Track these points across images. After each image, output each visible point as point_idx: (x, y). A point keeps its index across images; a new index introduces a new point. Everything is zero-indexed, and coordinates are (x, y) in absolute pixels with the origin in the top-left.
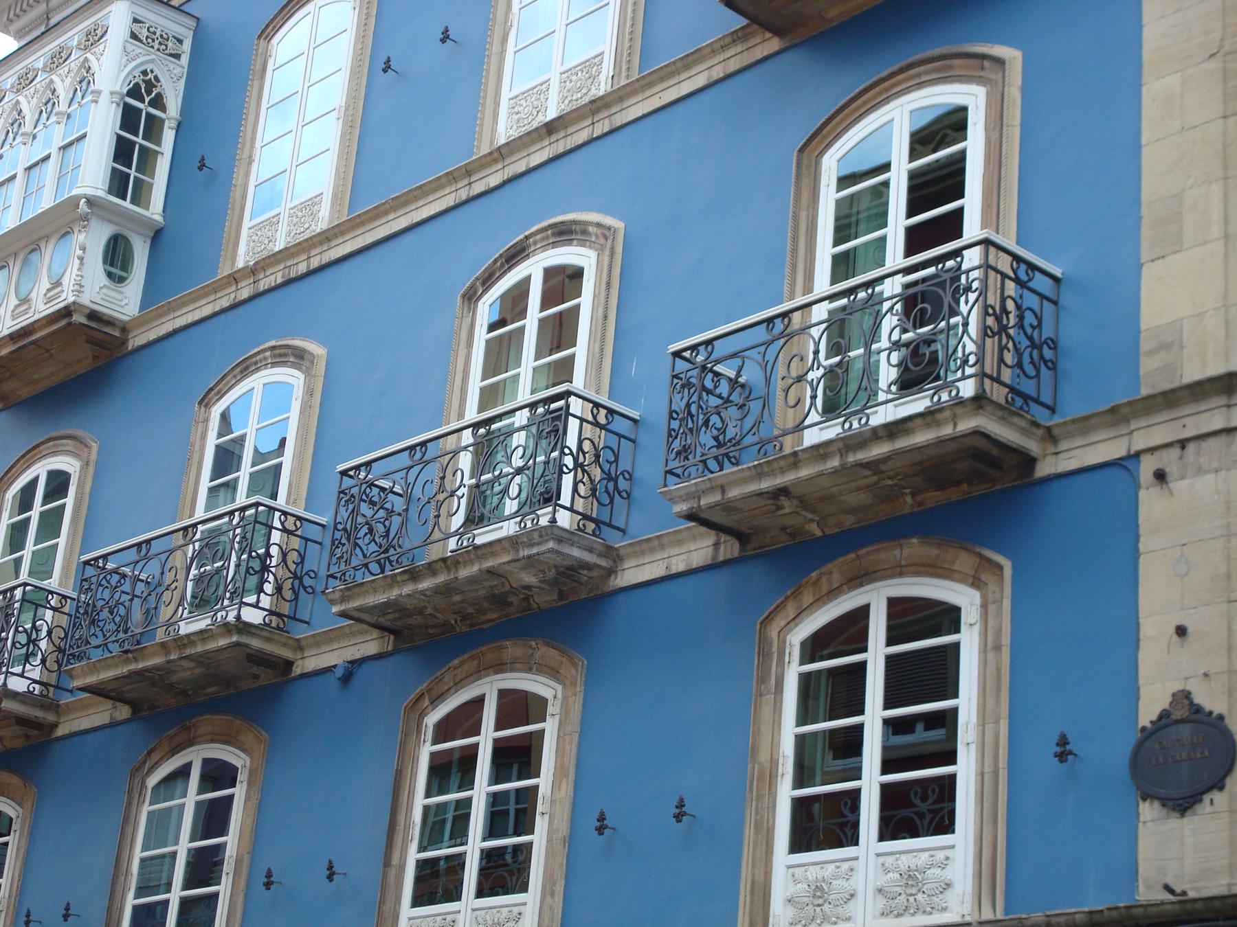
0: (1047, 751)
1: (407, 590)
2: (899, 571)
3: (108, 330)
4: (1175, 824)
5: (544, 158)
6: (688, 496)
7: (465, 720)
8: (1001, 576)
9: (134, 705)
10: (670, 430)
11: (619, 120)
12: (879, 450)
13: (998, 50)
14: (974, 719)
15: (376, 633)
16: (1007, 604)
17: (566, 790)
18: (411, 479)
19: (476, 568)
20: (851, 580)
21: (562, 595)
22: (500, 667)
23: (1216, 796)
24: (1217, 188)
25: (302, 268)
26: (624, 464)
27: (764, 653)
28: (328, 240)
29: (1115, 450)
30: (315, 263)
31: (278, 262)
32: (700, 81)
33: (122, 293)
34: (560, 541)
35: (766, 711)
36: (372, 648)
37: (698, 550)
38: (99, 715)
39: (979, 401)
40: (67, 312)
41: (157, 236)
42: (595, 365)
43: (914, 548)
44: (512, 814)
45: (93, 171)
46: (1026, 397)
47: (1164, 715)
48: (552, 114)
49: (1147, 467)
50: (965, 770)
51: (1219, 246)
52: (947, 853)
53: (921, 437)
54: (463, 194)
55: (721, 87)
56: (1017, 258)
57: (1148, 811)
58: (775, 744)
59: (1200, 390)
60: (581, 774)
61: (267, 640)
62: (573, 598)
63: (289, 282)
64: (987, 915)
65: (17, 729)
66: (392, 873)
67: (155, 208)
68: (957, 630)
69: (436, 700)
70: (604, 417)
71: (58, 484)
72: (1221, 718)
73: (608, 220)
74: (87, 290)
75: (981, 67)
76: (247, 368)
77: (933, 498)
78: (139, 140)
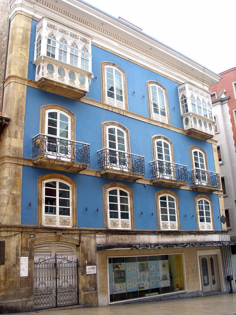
2: (171, 194)
36: (149, 184)
60: (179, 208)
76: (113, 124)
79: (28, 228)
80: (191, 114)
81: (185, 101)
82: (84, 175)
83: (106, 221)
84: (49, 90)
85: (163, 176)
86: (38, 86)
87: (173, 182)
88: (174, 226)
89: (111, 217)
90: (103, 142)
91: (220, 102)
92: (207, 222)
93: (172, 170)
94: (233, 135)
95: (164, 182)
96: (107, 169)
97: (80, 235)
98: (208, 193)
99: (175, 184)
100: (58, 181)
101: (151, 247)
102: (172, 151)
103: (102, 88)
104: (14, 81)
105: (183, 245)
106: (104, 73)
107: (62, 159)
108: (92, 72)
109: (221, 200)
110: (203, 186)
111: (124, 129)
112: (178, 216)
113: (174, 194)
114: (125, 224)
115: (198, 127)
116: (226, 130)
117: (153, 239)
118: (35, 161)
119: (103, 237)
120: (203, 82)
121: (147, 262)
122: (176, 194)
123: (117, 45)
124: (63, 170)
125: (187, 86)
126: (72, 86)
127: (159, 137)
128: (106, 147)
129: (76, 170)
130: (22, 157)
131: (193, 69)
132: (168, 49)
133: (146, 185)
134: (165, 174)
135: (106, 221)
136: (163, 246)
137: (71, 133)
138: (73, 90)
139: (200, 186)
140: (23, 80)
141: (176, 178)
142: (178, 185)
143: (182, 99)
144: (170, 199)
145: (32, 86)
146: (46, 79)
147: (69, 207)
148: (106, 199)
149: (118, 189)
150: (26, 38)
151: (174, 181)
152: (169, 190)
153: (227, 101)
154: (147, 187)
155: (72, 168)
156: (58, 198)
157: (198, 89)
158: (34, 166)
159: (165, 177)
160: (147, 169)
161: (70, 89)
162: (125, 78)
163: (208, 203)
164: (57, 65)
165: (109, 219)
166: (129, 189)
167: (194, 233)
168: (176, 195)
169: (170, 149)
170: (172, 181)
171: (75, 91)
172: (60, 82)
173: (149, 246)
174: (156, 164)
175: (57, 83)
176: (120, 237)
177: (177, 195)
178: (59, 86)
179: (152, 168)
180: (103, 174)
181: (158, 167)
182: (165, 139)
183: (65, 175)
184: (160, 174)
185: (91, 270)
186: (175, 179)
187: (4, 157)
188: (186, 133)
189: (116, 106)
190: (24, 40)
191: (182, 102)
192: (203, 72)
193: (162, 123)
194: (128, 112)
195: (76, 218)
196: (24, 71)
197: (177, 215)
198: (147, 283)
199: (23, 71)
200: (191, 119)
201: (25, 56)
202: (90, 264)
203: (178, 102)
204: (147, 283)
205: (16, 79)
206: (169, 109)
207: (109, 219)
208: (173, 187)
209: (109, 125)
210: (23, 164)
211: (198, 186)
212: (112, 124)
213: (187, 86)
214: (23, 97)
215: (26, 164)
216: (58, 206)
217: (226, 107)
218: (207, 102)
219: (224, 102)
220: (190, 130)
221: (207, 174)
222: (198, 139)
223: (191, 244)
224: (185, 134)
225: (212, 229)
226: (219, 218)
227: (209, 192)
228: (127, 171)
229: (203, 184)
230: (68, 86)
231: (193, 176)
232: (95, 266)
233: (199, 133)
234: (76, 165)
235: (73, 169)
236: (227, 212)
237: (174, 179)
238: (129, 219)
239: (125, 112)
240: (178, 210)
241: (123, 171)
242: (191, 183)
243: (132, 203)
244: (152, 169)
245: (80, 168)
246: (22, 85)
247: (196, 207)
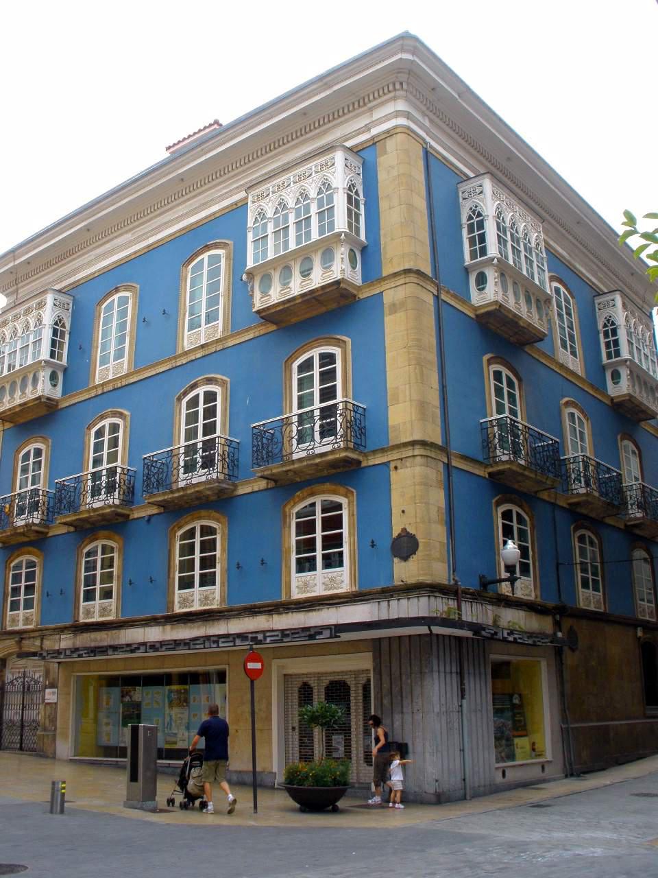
0: (368, 546)
1: (170, 496)
2: (323, 492)
3: (52, 403)
4: (403, 564)
5: (201, 356)
6: (261, 471)
7: (191, 534)
8: (353, 495)
9: (75, 527)
10: (253, 451)
12: (318, 460)
13: (344, 338)
14: (347, 535)
15: (156, 507)
16: (355, 503)
17: (225, 556)
18: (168, 461)
21: (219, 497)
22: (200, 518)
23: (413, 556)
24: (407, 386)
25: (119, 385)
26: (236, 457)
27: (285, 516)
28: (128, 376)
29: (384, 460)
30: (124, 384)
31: (111, 383)
32: (251, 336)
33: (310, 279)
34: (219, 483)
35: (287, 532)
37: (262, 484)
38: (64, 530)
39: (346, 449)
40: (39, 398)
41: (65, 370)
42: (223, 424)
43: (327, 486)
44: (208, 562)
45: (45, 354)
46: (358, 445)
47: (399, 535)
48: (203, 342)
49: (392, 465)
50: (346, 549)
51: (409, 403)
53: (330, 457)
56: (354, 405)
57: (396, 560)
58: (290, 543)
59: (405, 445)
60: (230, 551)
61: (122, 509)
62: (222, 497)
63: (114, 390)
64: (354, 589)
65: (35, 534)
66: (171, 580)
67: (64, 362)
68: (341, 510)
69: (180, 528)
70: (229, 443)
71: (38, 453)
72: (414, 535)
73: (224, 378)
74: (46, 390)
75: (340, 343)
77: (333, 471)
78: (58, 339)
80: (628, 363)
88: (206, 598)
97: (42, 640)
101: (65, 655)
105: (128, 649)
107: (194, 481)
111: (520, 380)
117: (154, 634)
119: (70, 638)
121: (186, 687)
123: (128, 237)
131: (304, 113)
132: (203, 147)
136: (86, 651)
138: (25, 406)
152: (328, 484)
164: (295, 259)
165: (581, 590)
167: (266, 609)
173: (61, 653)
176: (394, 615)
185: (51, 696)
192: (328, 92)
198: (183, 735)
202: (52, 686)
204: (183, 735)
223: (148, 644)
232: (55, 690)
238: (200, 586)
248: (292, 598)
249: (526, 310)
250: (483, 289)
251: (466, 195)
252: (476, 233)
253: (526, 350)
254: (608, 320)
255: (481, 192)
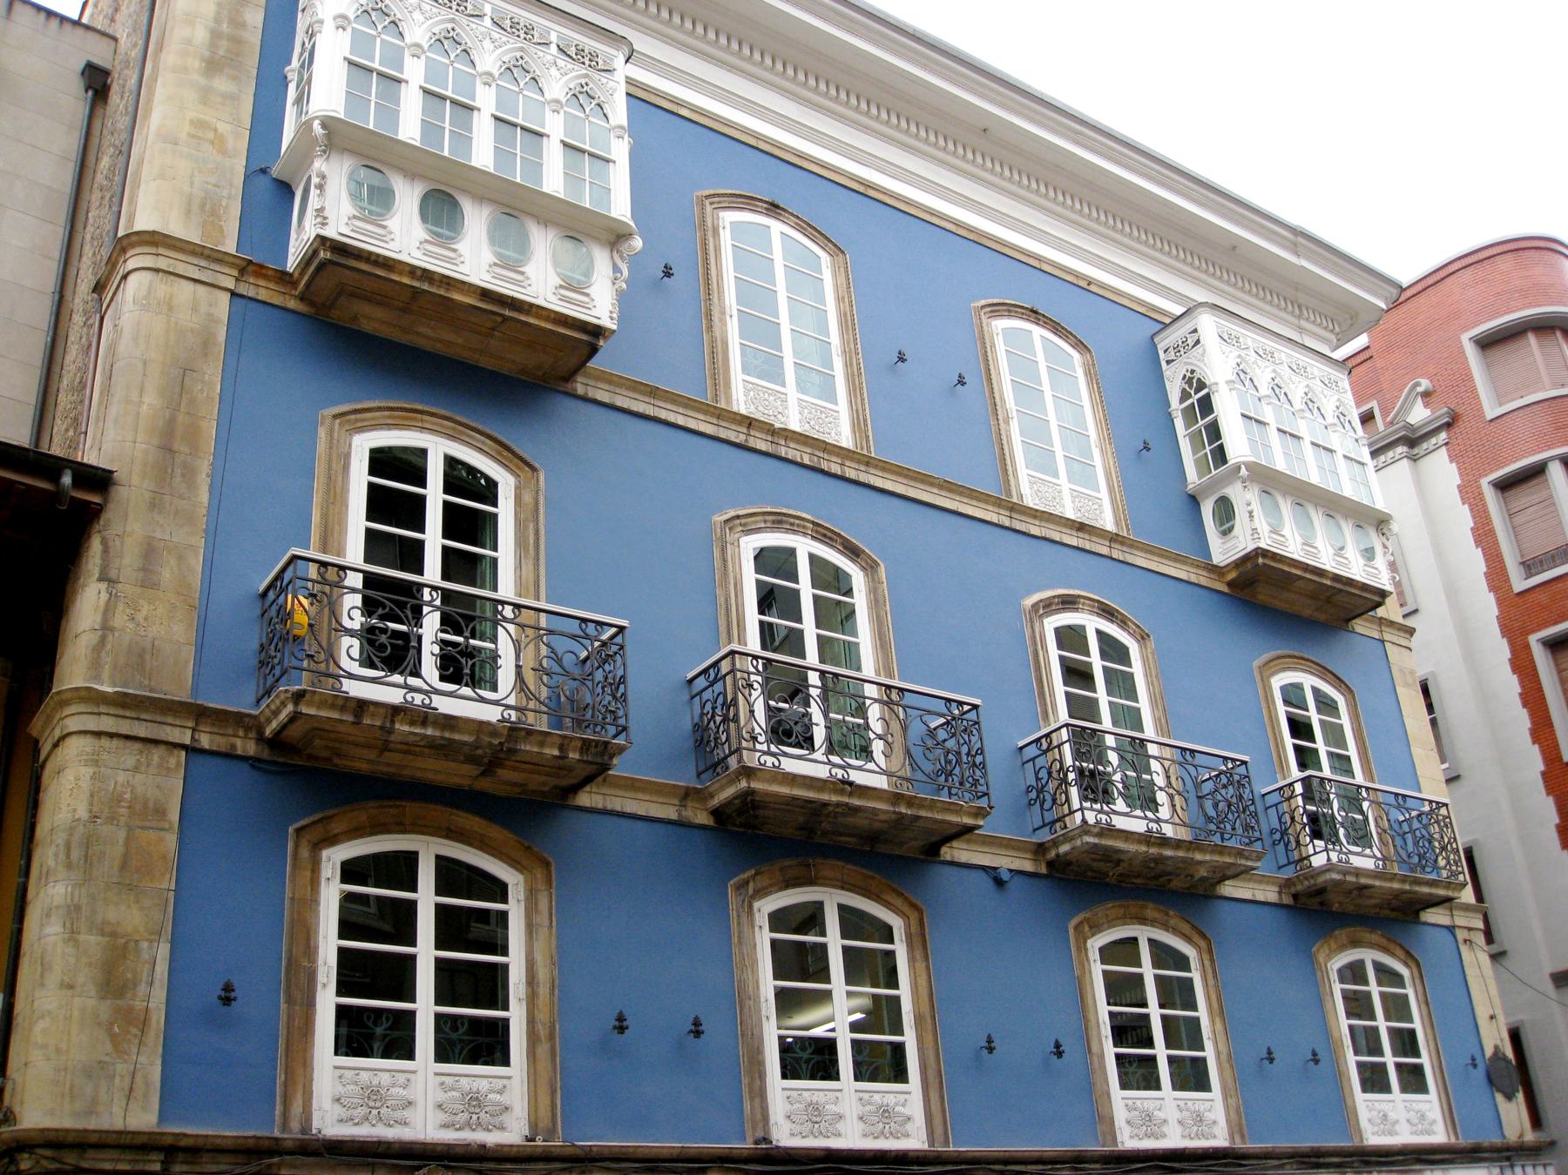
2: (1166, 927)
11: (1130, 559)
19: (437, 733)
20: (356, 829)
32: (1183, 575)
36: (1028, 866)
52: (505, 1082)
54: (1007, 522)
55: (1190, 587)
60: (1220, 1011)
76: (780, 522)
79: (208, 1151)
80: (1243, 471)
81: (1206, 405)
82: (605, 812)
83: (757, 1100)
84: (373, 319)
85: (1104, 817)
86: (302, 298)
87: (1168, 853)
89: (788, 1072)
90: (722, 622)
91: (1405, 449)
92: (1404, 1090)
93: (1160, 781)
94: (1495, 611)
95: (1119, 851)
96: (748, 772)
98: (1391, 914)
99: (1184, 860)
100: (428, 851)
102: (1149, 684)
103: (710, 327)
104: (148, 261)
106: (717, 249)
108: (632, 224)
109: (1476, 960)
110: (1358, 872)
111: (853, 552)
112: (1224, 1057)
113: (1186, 928)
114: (886, 1113)
115: (1291, 541)
116: (1452, 593)
118: (269, 721)
120: (1299, 317)
122: (1194, 927)
124: (465, 782)
125: (1207, 324)
126: (511, 293)
127: (1068, 603)
128: (742, 640)
129: (544, 784)
130: (183, 695)
133: (1005, 876)
134: (1120, 805)
135: (757, 1100)
137: (519, 566)
139: (1335, 876)
140: (208, 258)
141: (1184, 825)
142: (1203, 872)
143: (1185, 396)
144: (1163, 955)
145: (263, 295)
146: (340, 248)
147: (506, 1008)
148: (755, 962)
149: (832, 900)
150: (237, 41)
151: (1177, 844)
153: (1443, 435)
154: (1016, 885)
155: (514, 769)
156: (426, 952)
157: (1271, 344)
158: (266, 754)
159: (1120, 823)
160: (1004, 779)
161: (501, 312)
162: (842, 280)
163: (1397, 979)
165: (777, 1086)
166: (898, 902)
167: (1336, 1160)
168: (1198, 934)
169: (1137, 669)
170: (1164, 841)
171: (532, 321)
172: (429, 267)
174: (1059, 746)
175: (413, 271)
177: (1203, 935)
178: (426, 295)
179: (1036, 774)
180: (728, 811)
181: (1069, 761)
182: (1107, 613)
183: (481, 813)
184: (1087, 805)
186: (1184, 834)
187: (64, 697)
188: (1230, 584)
189: (795, 425)
190: (221, 53)
191: (1189, 414)
193: (1081, 527)
194: (868, 462)
195: (557, 1085)
196: (213, 213)
197: (1218, 1054)
199: (209, 210)
200: (1244, 497)
201: (222, 135)
203: (1160, 417)
205: (161, 250)
206: (1119, 453)
207: (777, 1086)
208: (1176, 884)
209: (758, 530)
210: (188, 742)
211: (1328, 876)
212: (779, 522)
213: (1207, 324)
214: (207, 344)
215: (211, 742)
216: (425, 1006)
217: (1441, 469)
218: (1329, 406)
219: (1425, 446)
220: (1249, 565)
221: (1372, 802)
222: (1296, 607)
224: (1225, 589)
225: (1439, 1136)
226: (1475, 1066)
227: (1394, 914)
228: (881, 782)
229: (1358, 862)
230: (486, 294)
231: (1293, 819)
233: (1300, 578)
234: (542, 744)
235: (523, 771)
236: (1515, 1036)
237: (1175, 832)
239: (852, 460)
240: (1218, 1020)
241: (851, 784)
242: (1283, 861)
243: (923, 982)
244: (1038, 779)
245: (570, 769)
246: (201, 289)
247: (1328, 1006)
248: (1120, 1147)
249: (1299, 540)
250: (1231, 529)
251: (1172, 356)
252: (1201, 423)
253: (1359, 629)
254: (1189, 382)
255: (1198, 342)
